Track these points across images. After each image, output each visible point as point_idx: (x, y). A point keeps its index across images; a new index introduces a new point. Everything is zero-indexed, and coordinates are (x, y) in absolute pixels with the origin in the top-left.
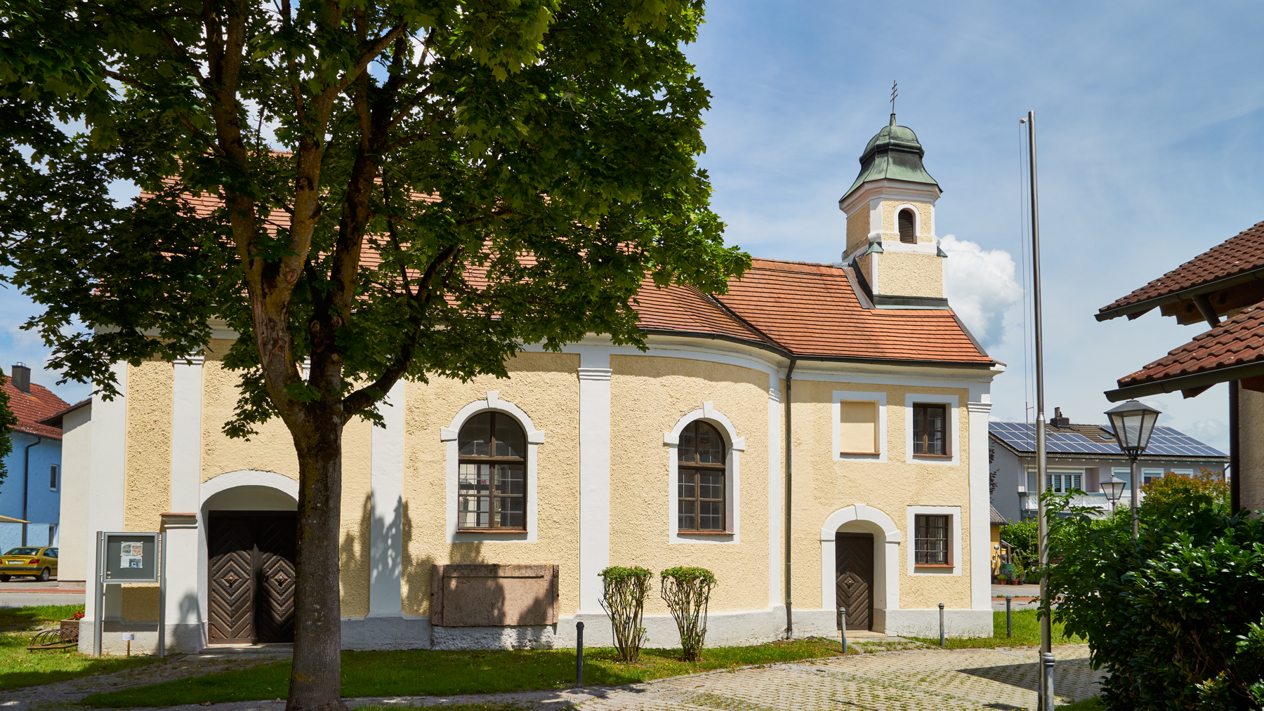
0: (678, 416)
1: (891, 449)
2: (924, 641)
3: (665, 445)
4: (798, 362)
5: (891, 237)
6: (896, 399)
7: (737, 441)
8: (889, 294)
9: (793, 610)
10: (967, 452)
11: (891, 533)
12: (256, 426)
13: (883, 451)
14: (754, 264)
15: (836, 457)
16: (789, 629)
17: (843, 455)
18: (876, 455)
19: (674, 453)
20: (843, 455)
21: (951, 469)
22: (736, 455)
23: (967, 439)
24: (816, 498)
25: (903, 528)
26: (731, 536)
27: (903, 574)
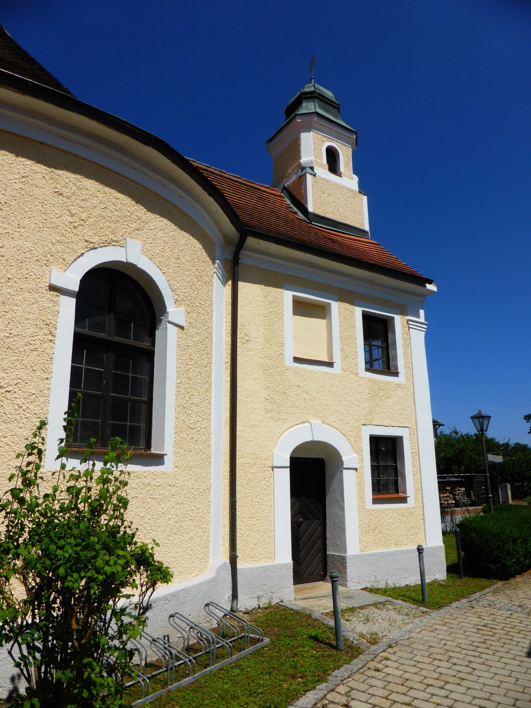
0: (80, 247)
1: (345, 358)
2: (385, 592)
3: (53, 288)
4: (251, 241)
5: (321, 165)
6: (348, 297)
7: (174, 312)
8: (322, 214)
9: (239, 566)
10: (410, 368)
11: (348, 458)
12: (23, 462)
13: (337, 359)
14: (151, 639)
15: (289, 362)
16: (235, 596)
17: (297, 360)
18: (330, 364)
19: (68, 307)
20: (297, 360)
21: (399, 385)
22: (172, 332)
23: (409, 356)
24: (267, 411)
25: (359, 451)
26: (158, 459)
27: (361, 508)
